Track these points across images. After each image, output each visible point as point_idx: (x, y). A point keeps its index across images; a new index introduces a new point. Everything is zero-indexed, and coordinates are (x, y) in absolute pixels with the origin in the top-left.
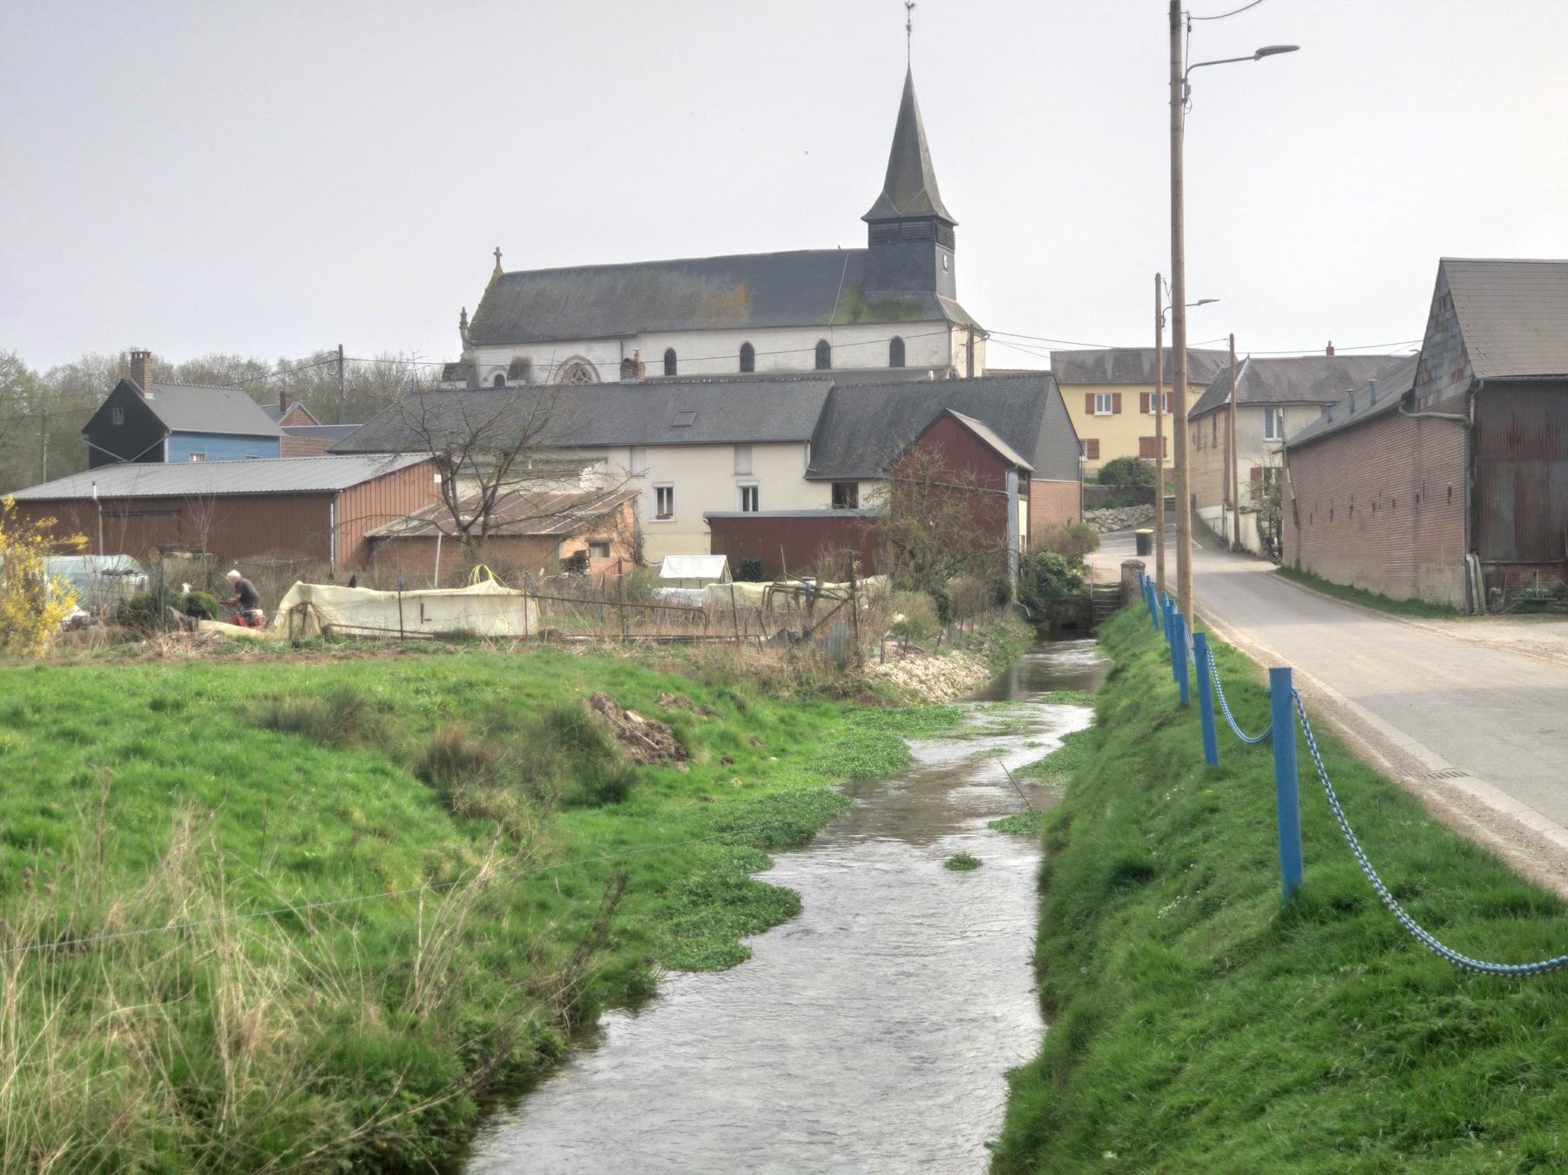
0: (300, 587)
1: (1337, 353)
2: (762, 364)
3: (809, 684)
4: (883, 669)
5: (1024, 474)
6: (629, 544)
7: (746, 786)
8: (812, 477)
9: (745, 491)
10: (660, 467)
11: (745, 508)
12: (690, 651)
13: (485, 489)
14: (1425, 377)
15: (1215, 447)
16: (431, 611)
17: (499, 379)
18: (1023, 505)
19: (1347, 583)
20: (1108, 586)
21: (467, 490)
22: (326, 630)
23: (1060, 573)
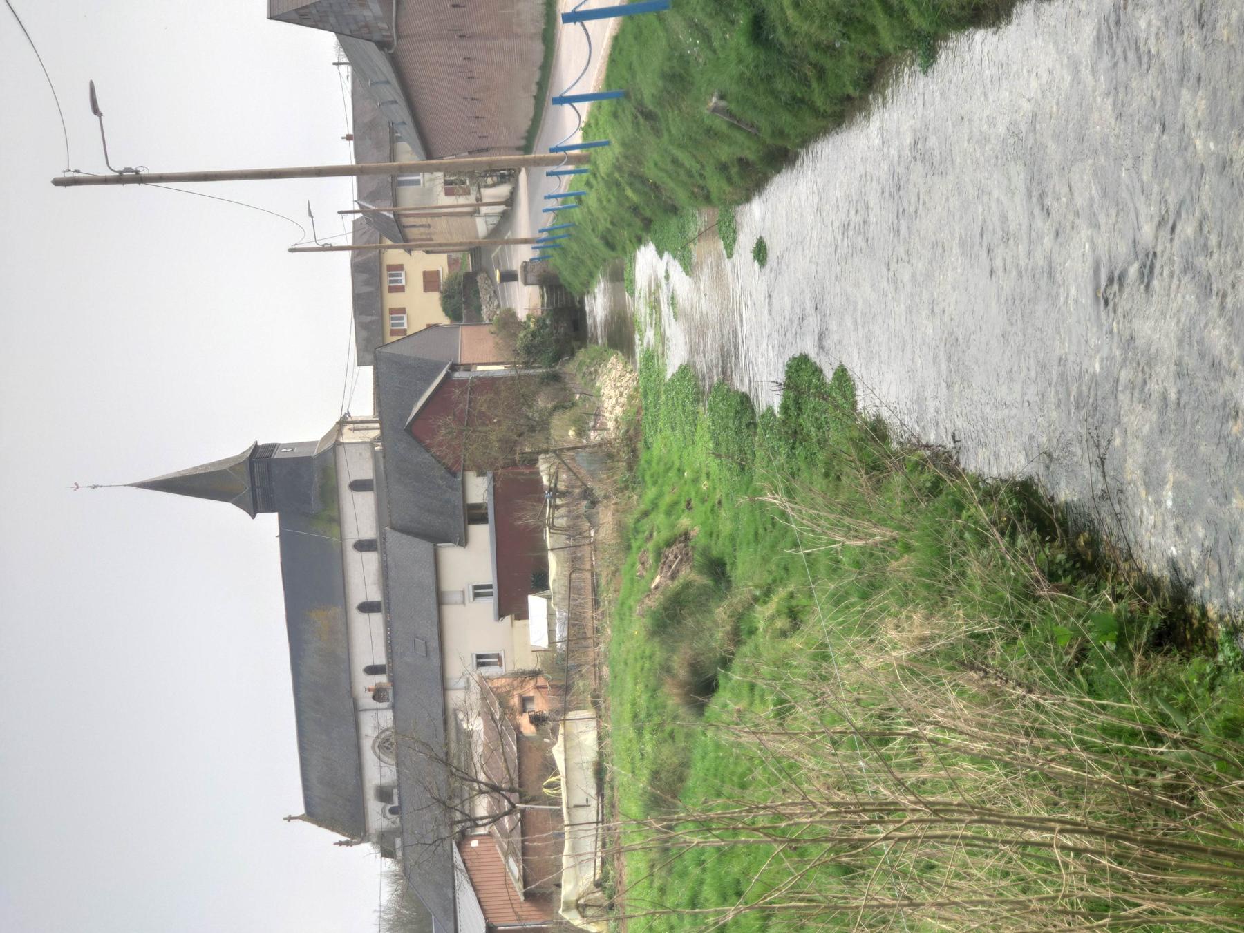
0: (564, 911)
1: (351, 132)
2: (375, 596)
3: (626, 481)
4: (611, 425)
5: (454, 367)
6: (522, 682)
7: (708, 478)
8: (463, 541)
9: (476, 595)
10: (459, 666)
11: (490, 595)
12: (603, 581)
13: (481, 792)
14: (364, 31)
15: (429, 226)
16: (579, 799)
17: (393, 811)
18: (480, 368)
19: (533, 101)
20: (542, 297)
21: (482, 806)
22: (598, 885)
23: (534, 335)
